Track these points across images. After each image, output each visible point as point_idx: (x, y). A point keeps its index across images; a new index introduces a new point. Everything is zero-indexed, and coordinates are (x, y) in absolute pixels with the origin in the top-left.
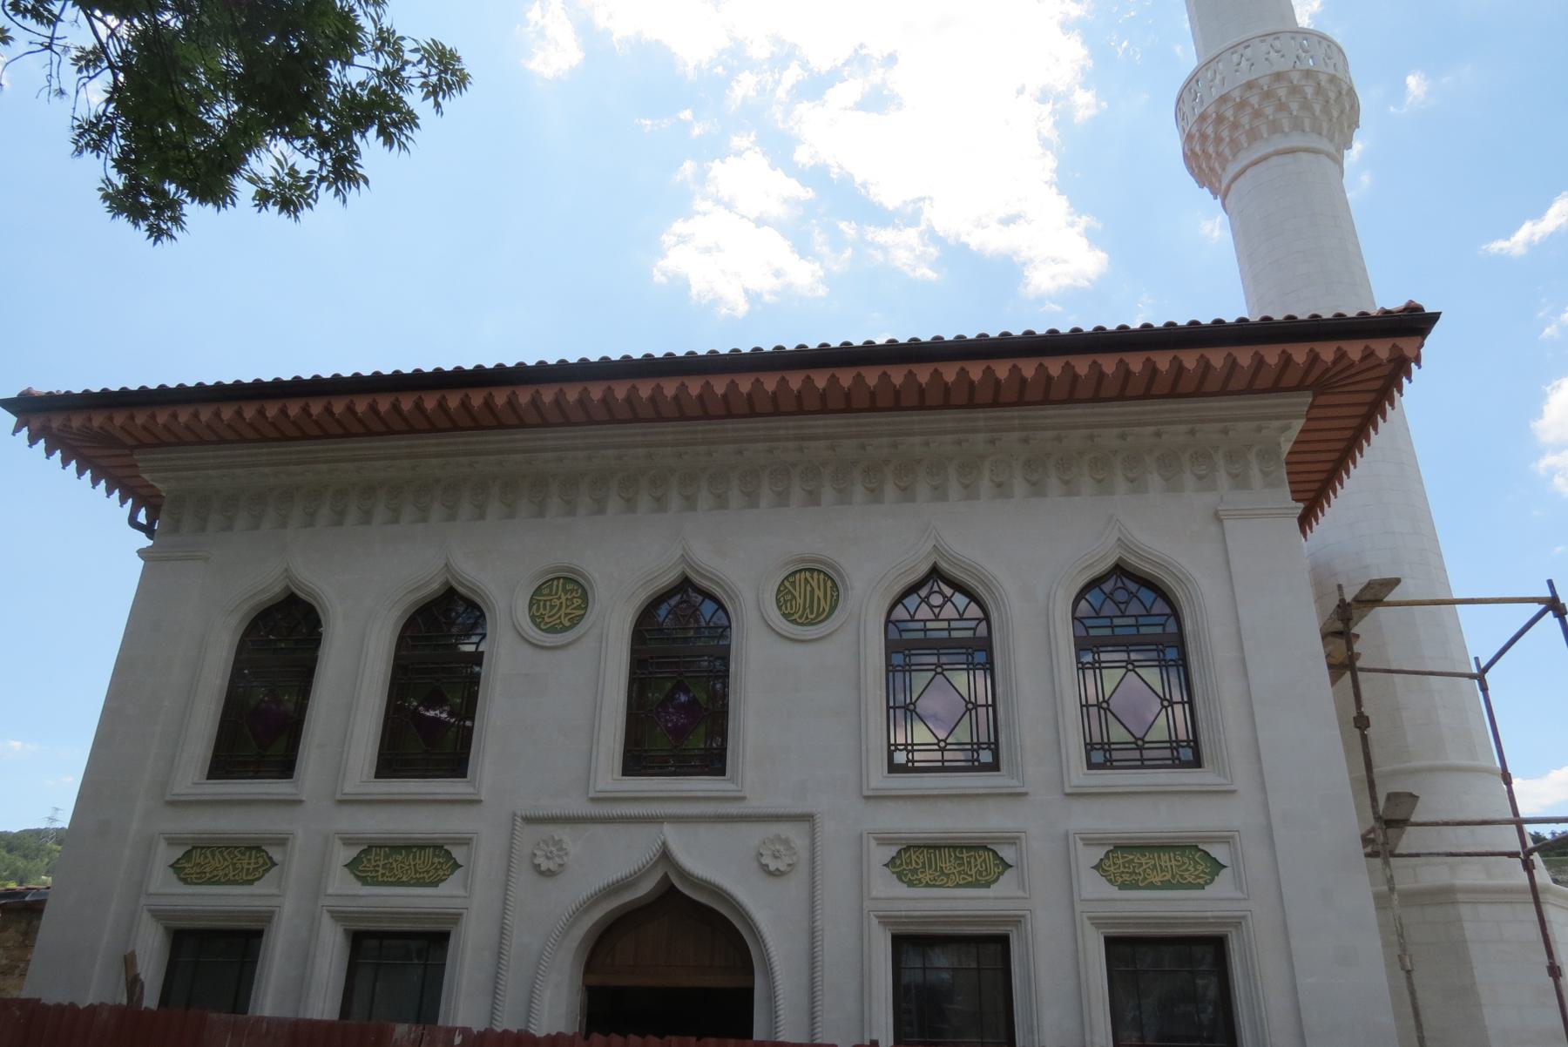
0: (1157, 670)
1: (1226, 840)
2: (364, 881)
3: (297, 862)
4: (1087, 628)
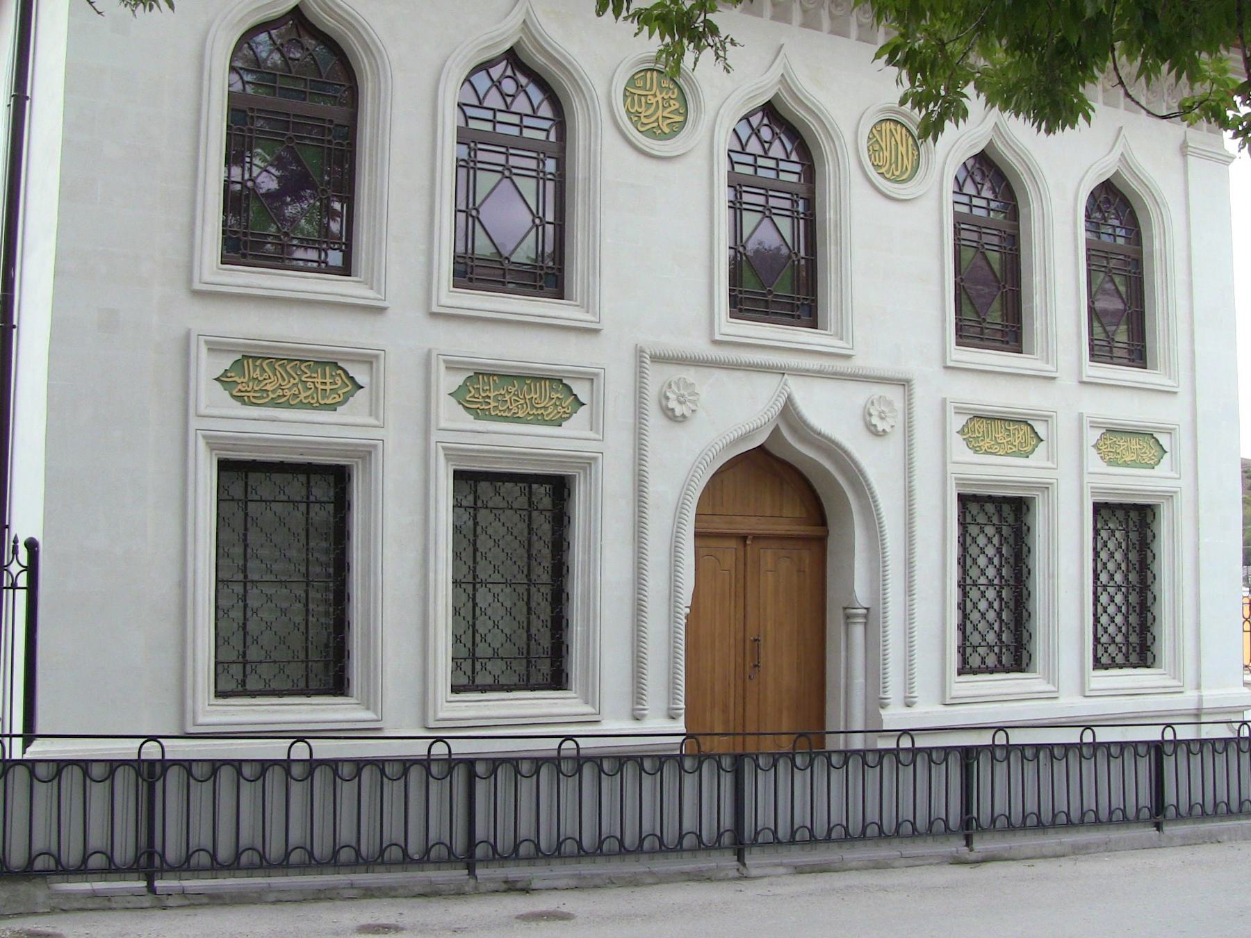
0: (533, 182)
1: (1169, 432)
2: (477, 414)
3: (399, 382)
4: (467, 118)
